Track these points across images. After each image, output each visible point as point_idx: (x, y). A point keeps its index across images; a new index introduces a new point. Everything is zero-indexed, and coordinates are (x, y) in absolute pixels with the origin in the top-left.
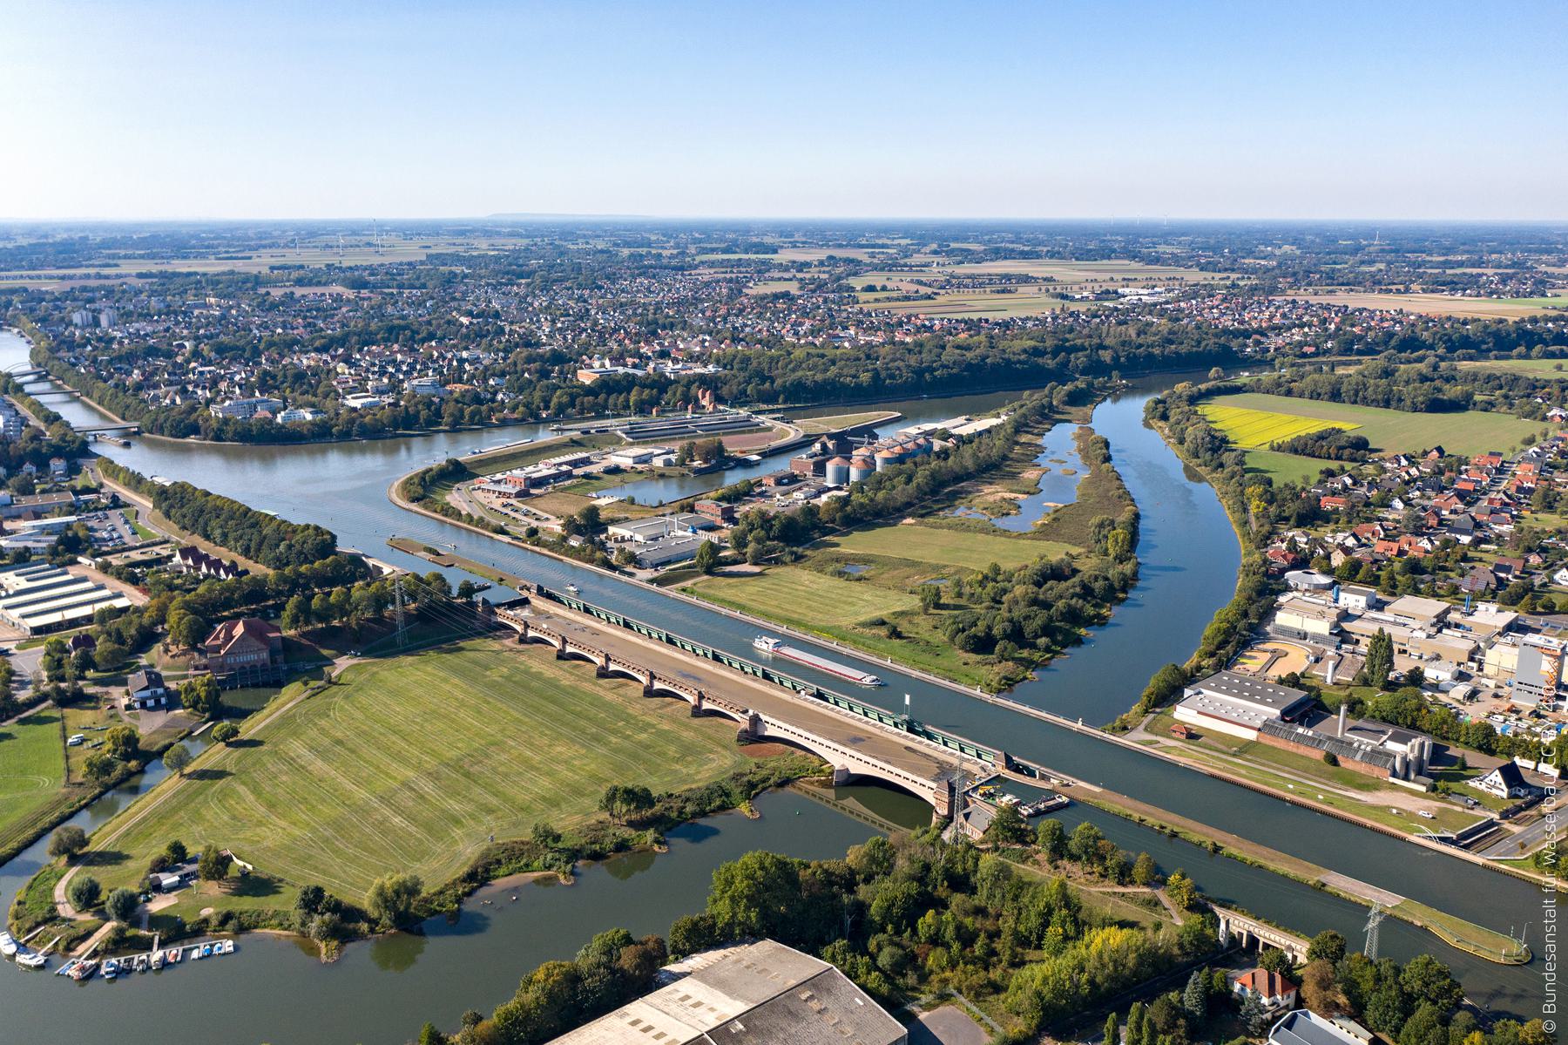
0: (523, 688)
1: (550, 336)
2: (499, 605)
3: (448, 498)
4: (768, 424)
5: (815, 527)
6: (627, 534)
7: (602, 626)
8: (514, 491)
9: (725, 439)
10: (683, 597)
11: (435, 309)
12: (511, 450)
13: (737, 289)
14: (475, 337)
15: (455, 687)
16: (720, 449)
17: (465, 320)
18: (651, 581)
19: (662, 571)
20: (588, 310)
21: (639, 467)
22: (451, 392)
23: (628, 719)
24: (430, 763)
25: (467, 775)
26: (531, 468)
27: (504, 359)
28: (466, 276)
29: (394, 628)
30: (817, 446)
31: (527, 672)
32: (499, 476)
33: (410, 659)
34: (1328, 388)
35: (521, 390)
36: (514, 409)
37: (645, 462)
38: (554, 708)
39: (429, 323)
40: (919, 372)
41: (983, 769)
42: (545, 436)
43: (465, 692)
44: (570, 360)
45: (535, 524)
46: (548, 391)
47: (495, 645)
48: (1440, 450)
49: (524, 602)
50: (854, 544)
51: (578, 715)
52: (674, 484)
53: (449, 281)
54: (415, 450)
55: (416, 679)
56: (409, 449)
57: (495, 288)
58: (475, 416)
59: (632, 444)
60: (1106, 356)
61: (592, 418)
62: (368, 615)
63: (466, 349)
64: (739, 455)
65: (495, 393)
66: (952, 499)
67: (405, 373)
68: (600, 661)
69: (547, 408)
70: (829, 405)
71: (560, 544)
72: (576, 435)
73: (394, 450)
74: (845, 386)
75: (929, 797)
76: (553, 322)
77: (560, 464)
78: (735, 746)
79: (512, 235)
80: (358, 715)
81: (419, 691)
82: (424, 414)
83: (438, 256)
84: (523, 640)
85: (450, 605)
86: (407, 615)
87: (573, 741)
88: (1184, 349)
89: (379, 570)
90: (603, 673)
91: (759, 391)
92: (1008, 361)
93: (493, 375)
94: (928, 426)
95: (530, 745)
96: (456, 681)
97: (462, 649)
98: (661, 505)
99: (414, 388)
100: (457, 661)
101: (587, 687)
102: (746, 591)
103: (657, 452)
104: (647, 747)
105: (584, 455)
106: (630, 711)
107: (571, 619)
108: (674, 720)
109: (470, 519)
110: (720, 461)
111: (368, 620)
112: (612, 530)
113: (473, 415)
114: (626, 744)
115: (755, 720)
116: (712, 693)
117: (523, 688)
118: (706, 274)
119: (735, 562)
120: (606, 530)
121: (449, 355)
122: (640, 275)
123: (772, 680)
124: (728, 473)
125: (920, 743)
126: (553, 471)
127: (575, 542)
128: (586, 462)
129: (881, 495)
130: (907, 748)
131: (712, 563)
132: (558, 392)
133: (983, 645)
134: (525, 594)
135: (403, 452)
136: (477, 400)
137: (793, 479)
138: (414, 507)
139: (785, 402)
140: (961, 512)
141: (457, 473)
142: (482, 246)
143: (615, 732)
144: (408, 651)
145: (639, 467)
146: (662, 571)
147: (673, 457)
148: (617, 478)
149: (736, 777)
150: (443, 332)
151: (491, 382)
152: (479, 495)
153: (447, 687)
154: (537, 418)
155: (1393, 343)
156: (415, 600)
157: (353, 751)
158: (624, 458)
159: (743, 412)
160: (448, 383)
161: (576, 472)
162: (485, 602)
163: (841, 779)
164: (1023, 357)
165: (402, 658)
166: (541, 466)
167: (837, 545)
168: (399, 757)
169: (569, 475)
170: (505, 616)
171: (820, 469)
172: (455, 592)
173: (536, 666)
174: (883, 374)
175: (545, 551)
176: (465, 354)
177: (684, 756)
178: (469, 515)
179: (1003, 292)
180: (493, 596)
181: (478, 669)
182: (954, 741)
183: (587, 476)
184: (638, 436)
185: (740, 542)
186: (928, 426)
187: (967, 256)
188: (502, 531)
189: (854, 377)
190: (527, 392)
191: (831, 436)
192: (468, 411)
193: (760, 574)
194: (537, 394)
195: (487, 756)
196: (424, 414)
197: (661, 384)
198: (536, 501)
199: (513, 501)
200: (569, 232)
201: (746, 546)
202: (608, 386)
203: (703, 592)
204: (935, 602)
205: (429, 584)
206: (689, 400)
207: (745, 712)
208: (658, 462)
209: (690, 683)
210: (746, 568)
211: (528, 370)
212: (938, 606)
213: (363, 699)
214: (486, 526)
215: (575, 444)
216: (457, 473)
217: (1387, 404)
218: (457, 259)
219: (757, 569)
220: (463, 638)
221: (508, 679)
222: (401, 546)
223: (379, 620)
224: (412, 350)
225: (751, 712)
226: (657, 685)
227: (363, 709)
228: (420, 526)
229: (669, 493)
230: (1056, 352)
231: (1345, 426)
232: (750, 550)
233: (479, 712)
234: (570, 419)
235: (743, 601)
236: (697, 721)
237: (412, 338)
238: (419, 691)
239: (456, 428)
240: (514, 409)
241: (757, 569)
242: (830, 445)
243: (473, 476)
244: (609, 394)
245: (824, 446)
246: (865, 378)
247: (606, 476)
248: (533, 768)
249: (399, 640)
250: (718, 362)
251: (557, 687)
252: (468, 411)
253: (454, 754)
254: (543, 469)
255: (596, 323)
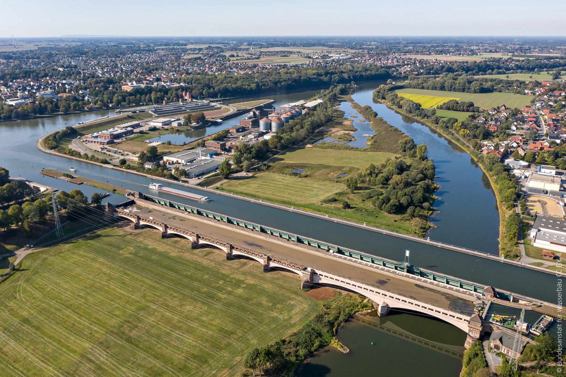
0: (145, 262)
1: (103, 74)
2: (118, 206)
3: (70, 147)
4: (219, 106)
5: (268, 151)
6: (175, 160)
7: (185, 215)
8: (106, 141)
9: (205, 113)
10: (218, 192)
11: (46, 65)
12: (99, 122)
13: (178, 58)
14: (65, 75)
15: (101, 265)
16: (203, 117)
17: (61, 69)
18: (200, 184)
19: (202, 179)
20: (117, 65)
21: (166, 127)
22: (61, 97)
23: (224, 277)
24: (100, 332)
25: (129, 340)
26: (111, 130)
27: (84, 83)
28: (57, 54)
29: (53, 226)
30: (252, 113)
31: (146, 249)
32: (95, 134)
33: (67, 246)
34: (439, 85)
35: (96, 95)
36: (96, 103)
37: (168, 125)
38: (174, 275)
39: (44, 70)
40: (276, 83)
41: (479, 298)
42: (112, 116)
43: (110, 268)
44: (116, 82)
45: (122, 157)
46: (108, 96)
47: (120, 231)
48: (504, 105)
49: (132, 203)
50: (290, 158)
51: (190, 278)
52: (183, 135)
53: (50, 56)
54: (46, 125)
55: (73, 257)
56: (43, 124)
57: (71, 58)
58: (76, 107)
59: (158, 117)
60: (345, 76)
61: (134, 106)
62: (36, 220)
63: (65, 79)
64: (212, 120)
65: (84, 97)
66: (322, 135)
67: (36, 90)
68: (192, 239)
69: (112, 102)
70: (242, 98)
71: (141, 168)
72: (130, 114)
73: (35, 125)
74: (245, 90)
75: (463, 326)
76: (102, 69)
77: (127, 127)
78: (302, 292)
79: (73, 41)
80: (37, 294)
81: (78, 270)
82: (49, 106)
83: (43, 48)
84: (137, 227)
85: (88, 210)
86: (61, 217)
87: (195, 300)
88: (373, 72)
89: (38, 190)
90: (196, 246)
91: (209, 93)
92: (310, 78)
93: (81, 89)
94: (293, 104)
95: (167, 307)
96: (102, 260)
97: (99, 236)
98: (185, 144)
99: (42, 95)
100: (98, 244)
101: (188, 256)
102: (252, 187)
103: (172, 120)
104: (247, 300)
105: (137, 122)
106: (223, 272)
107: (166, 215)
108: (254, 276)
109: (86, 156)
110: (204, 123)
111: (36, 222)
112: (165, 158)
113: (75, 106)
114: (231, 298)
115: (313, 273)
116: (276, 257)
117: (145, 262)
118: (162, 53)
119: (237, 171)
120: (162, 158)
121: (57, 82)
122: (134, 53)
123: (174, 207)
124: (207, 129)
125: (416, 279)
126: (123, 130)
127: (147, 166)
128: (138, 126)
129: (294, 134)
130: (416, 285)
131: (228, 173)
132: (116, 95)
133: (399, 209)
134: (132, 198)
135: (40, 126)
136: (75, 99)
137: (243, 129)
138: (53, 152)
139: (221, 97)
140: (327, 140)
141: (72, 133)
142: (63, 45)
143: (220, 289)
144: (66, 241)
145: (166, 127)
146: (202, 179)
147: (182, 122)
148: (157, 133)
149: (320, 318)
150: (54, 74)
151: (81, 92)
152: (89, 145)
153: (97, 265)
154: (108, 107)
155: (444, 70)
156: (65, 208)
157: (38, 329)
158: (157, 123)
159: (205, 102)
160: (59, 93)
161: (135, 131)
162: (109, 205)
163: (384, 312)
164: (315, 76)
165: (61, 246)
166: (116, 128)
167: (283, 159)
168: (74, 329)
169: (131, 132)
170: (124, 212)
171: (256, 124)
172: (90, 201)
173: (151, 245)
174: (261, 84)
175: (135, 172)
176: (64, 82)
177: (274, 305)
178: (86, 155)
179: (285, 56)
180: (114, 200)
181: (114, 249)
182: (368, 257)
183: (141, 132)
184: (160, 113)
185: (238, 161)
186: (293, 104)
187: (261, 46)
188: (106, 162)
189: (249, 85)
190: (100, 95)
191: (257, 109)
192: (72, 105)
193: (253, 177)
194: (105, 96)
195: (140, 321)
196: (49, 106)
197: (165, 91)
198: (118, 146)
199: (106, 146)
200: (100, 41)
201: (241, 162)
202: (137, 92)
203: (224, 189)
204: (355, 187)
205: (73, 197)
206: (179, 97)
207: (305, 269)
208: (175, 124)
209: (258, 250)
210: (243, 174)
211: (98, 86)
212: (357, 188)
213: (38, 280)
214: (97, 160)
215: (130, 118)
216: (72, 133)
217: (463, 90)
218: (52, 49)
219: (250, 174)
220: (97, 229)
221: (135, 254)
222: (48, 174)
223: (43, 222)
224: (38, 80)
225: (309, 269)
226: (235, 252)
227: (41, 289)
228: (56, 162)
229: (181, 139)
230: (326, 74)
231: (457, 99)
232: (245, 164)
233: (123, 283)
234: (123, 107)
235: (254, 193)
236: (269, 275)
237: (37, 76)
238: (78, 270)
239: (67, 113)
240: (96, 103)
241: (250, 174)
242: (257, 113)
243: (82, 135)
244: (141, 95)
245: (254, 113)
246: (253, 86)
247: (150, 132)
248: (176, 327)
249: (58, 233)
250: (185, 82)
251: (169, 258)
252: (72, 105)
253: (114, 321)
254: (118, 130)
255: (122, 70)
